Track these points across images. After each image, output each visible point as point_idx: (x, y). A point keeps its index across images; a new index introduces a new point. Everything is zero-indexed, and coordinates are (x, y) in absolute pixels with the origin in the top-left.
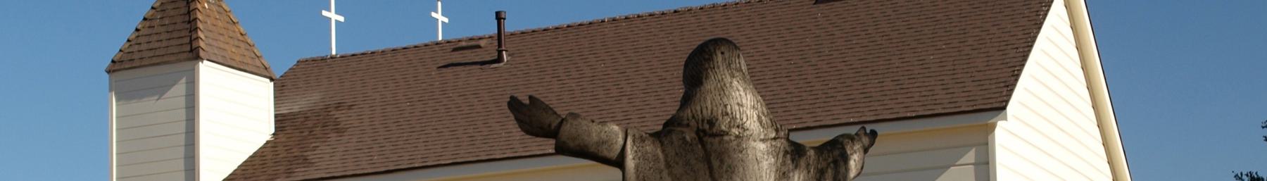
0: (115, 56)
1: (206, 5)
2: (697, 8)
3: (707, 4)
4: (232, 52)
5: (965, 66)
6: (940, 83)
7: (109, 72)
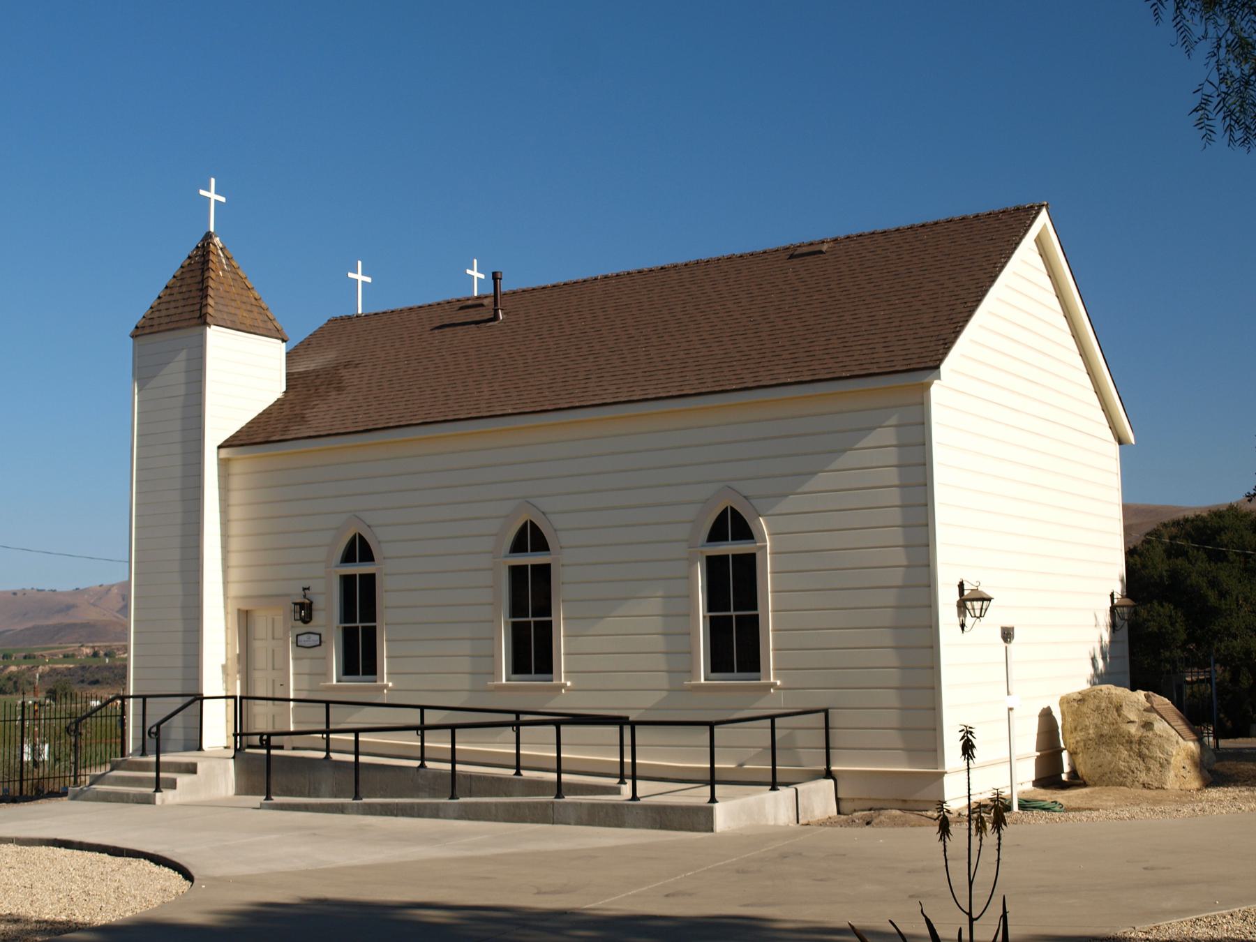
0: (139, 322)
1: (221, 273)
2: (682, 264)
3: (692, 260)
4: (243, 316)
5: (911, 323)
6: (883, 340)
7: (132, 337)
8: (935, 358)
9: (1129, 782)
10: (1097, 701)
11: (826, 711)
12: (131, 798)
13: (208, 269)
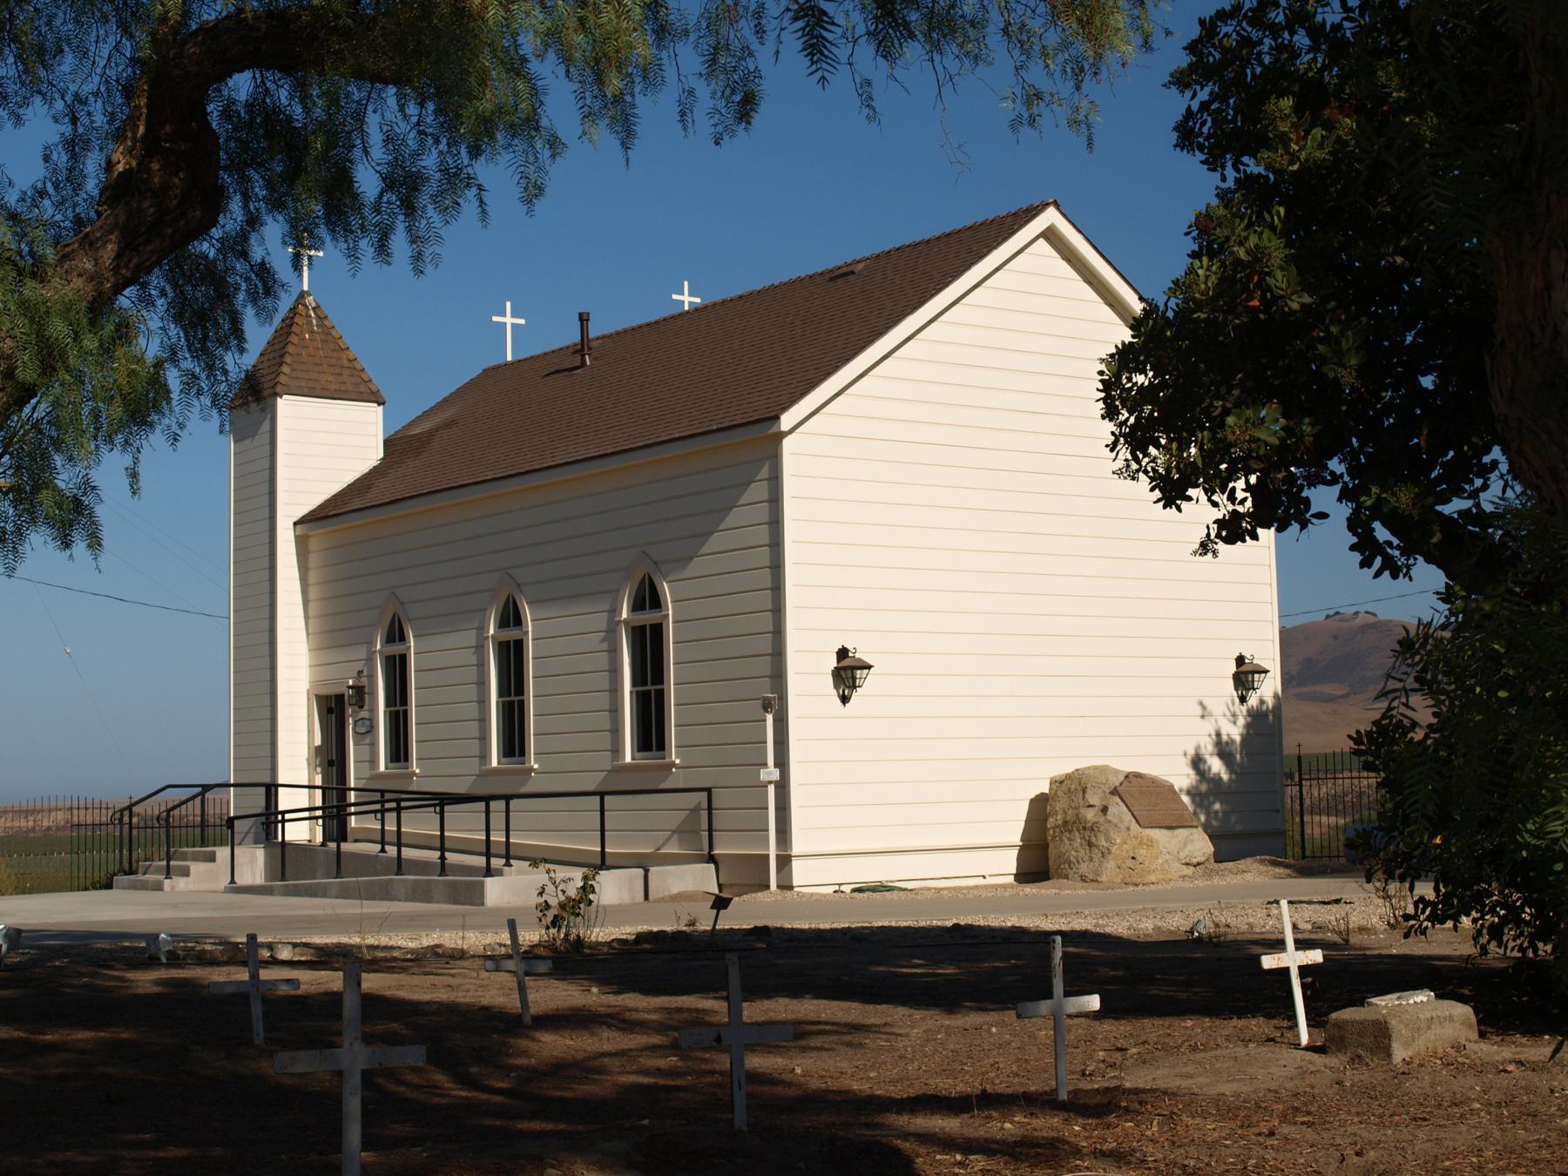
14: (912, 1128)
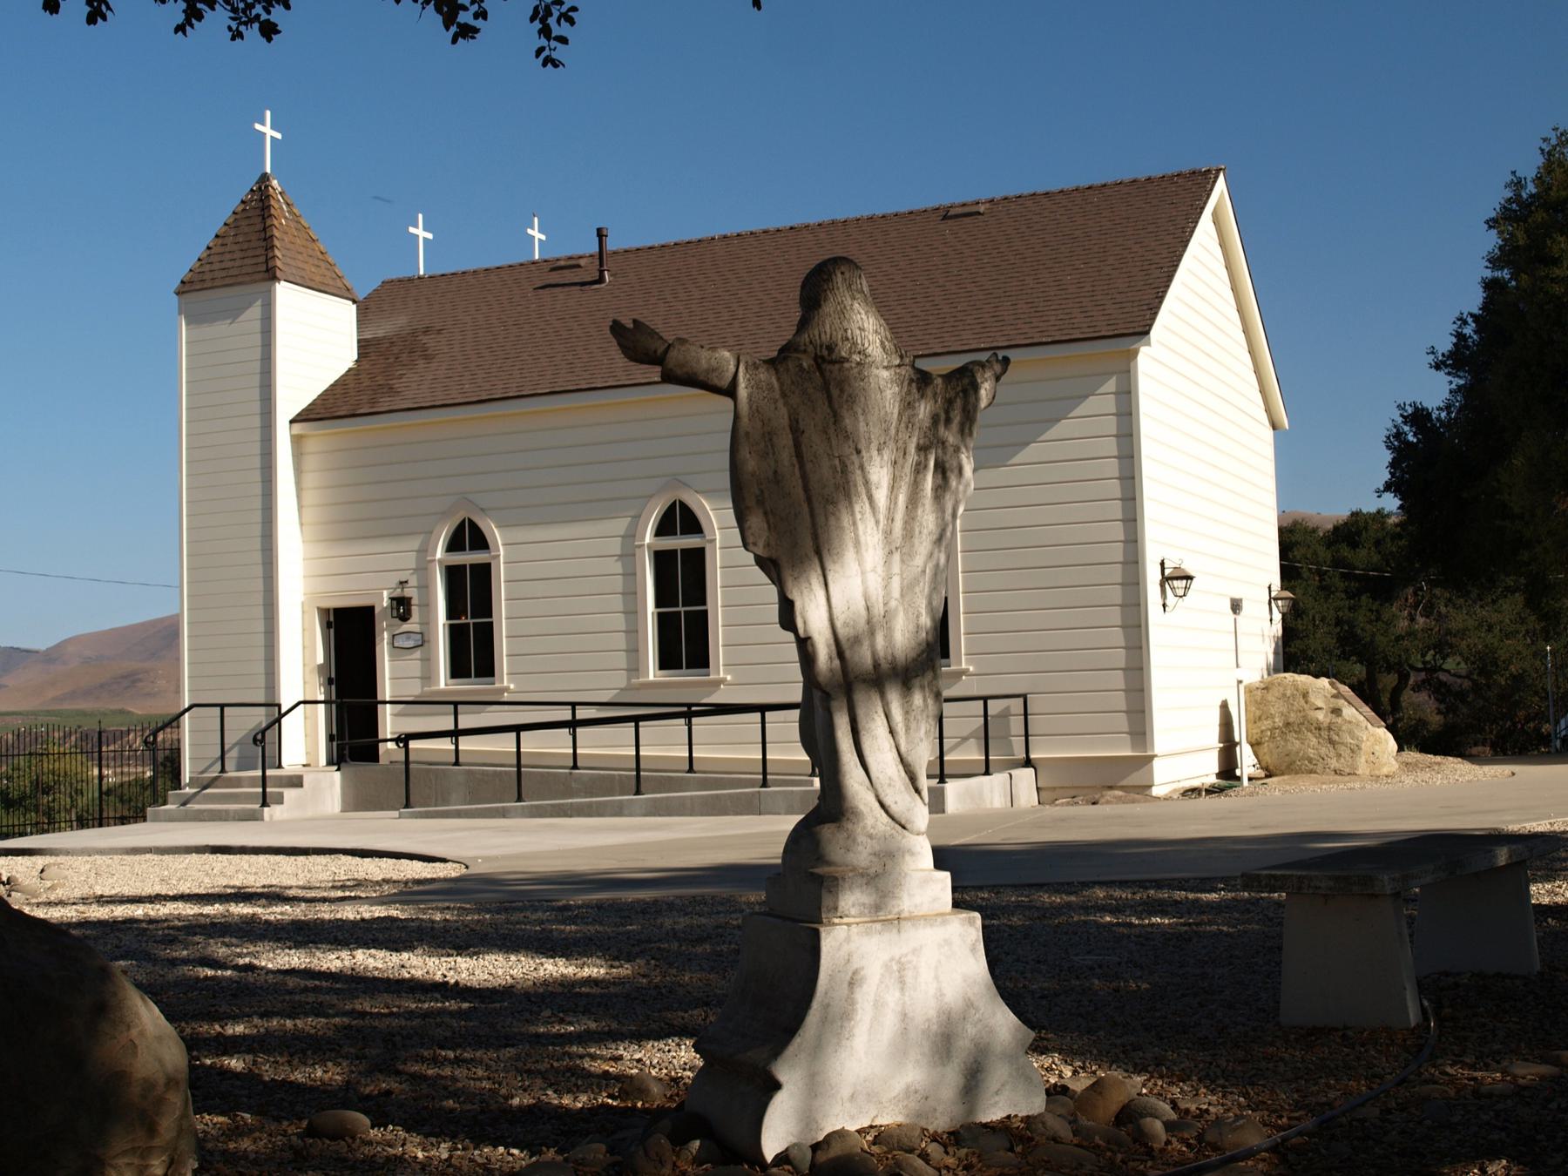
5: (1105, 287)
8: (1144, 323)
9: (1319, 768)
10: (1281, 689)
11: (1025, 697)
12: (232, 814)
13: (270, 216)
14: (387, 998)
